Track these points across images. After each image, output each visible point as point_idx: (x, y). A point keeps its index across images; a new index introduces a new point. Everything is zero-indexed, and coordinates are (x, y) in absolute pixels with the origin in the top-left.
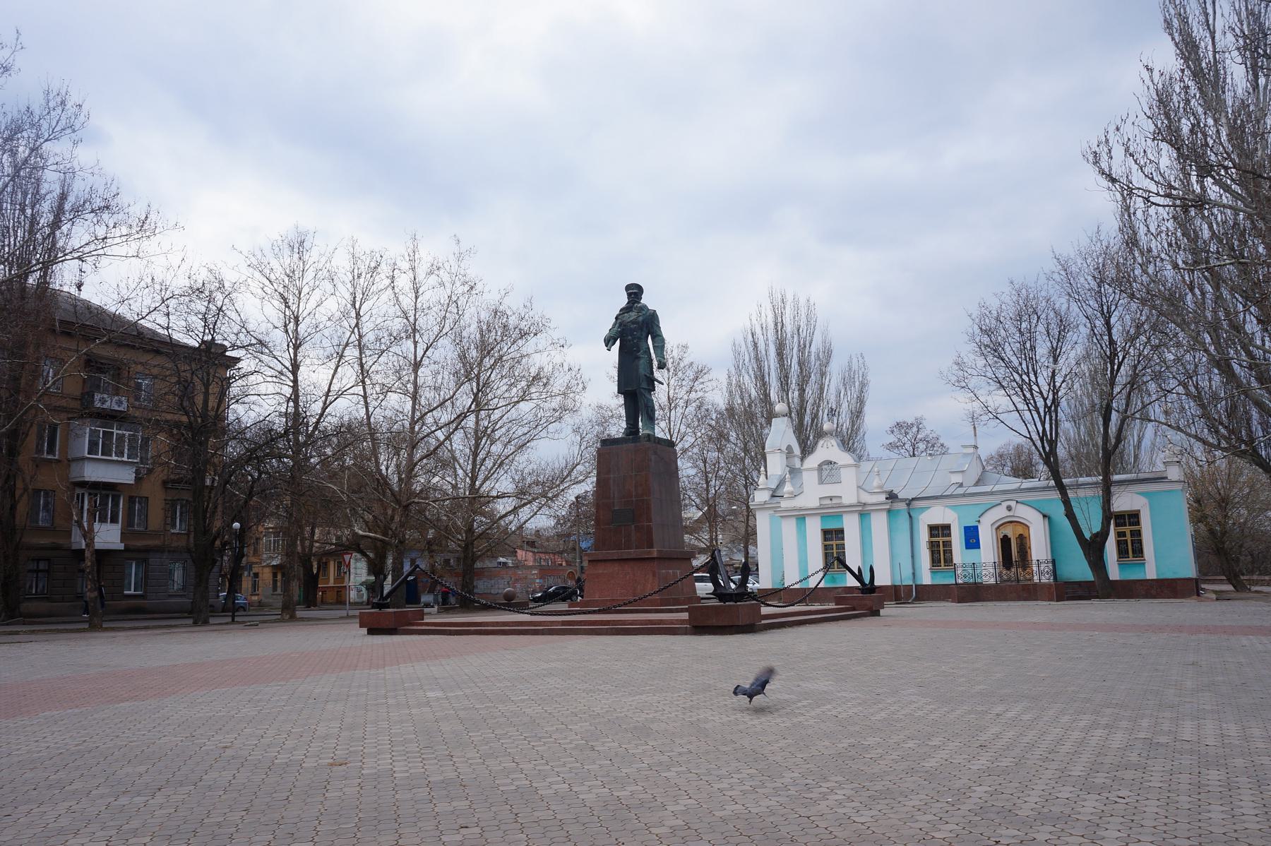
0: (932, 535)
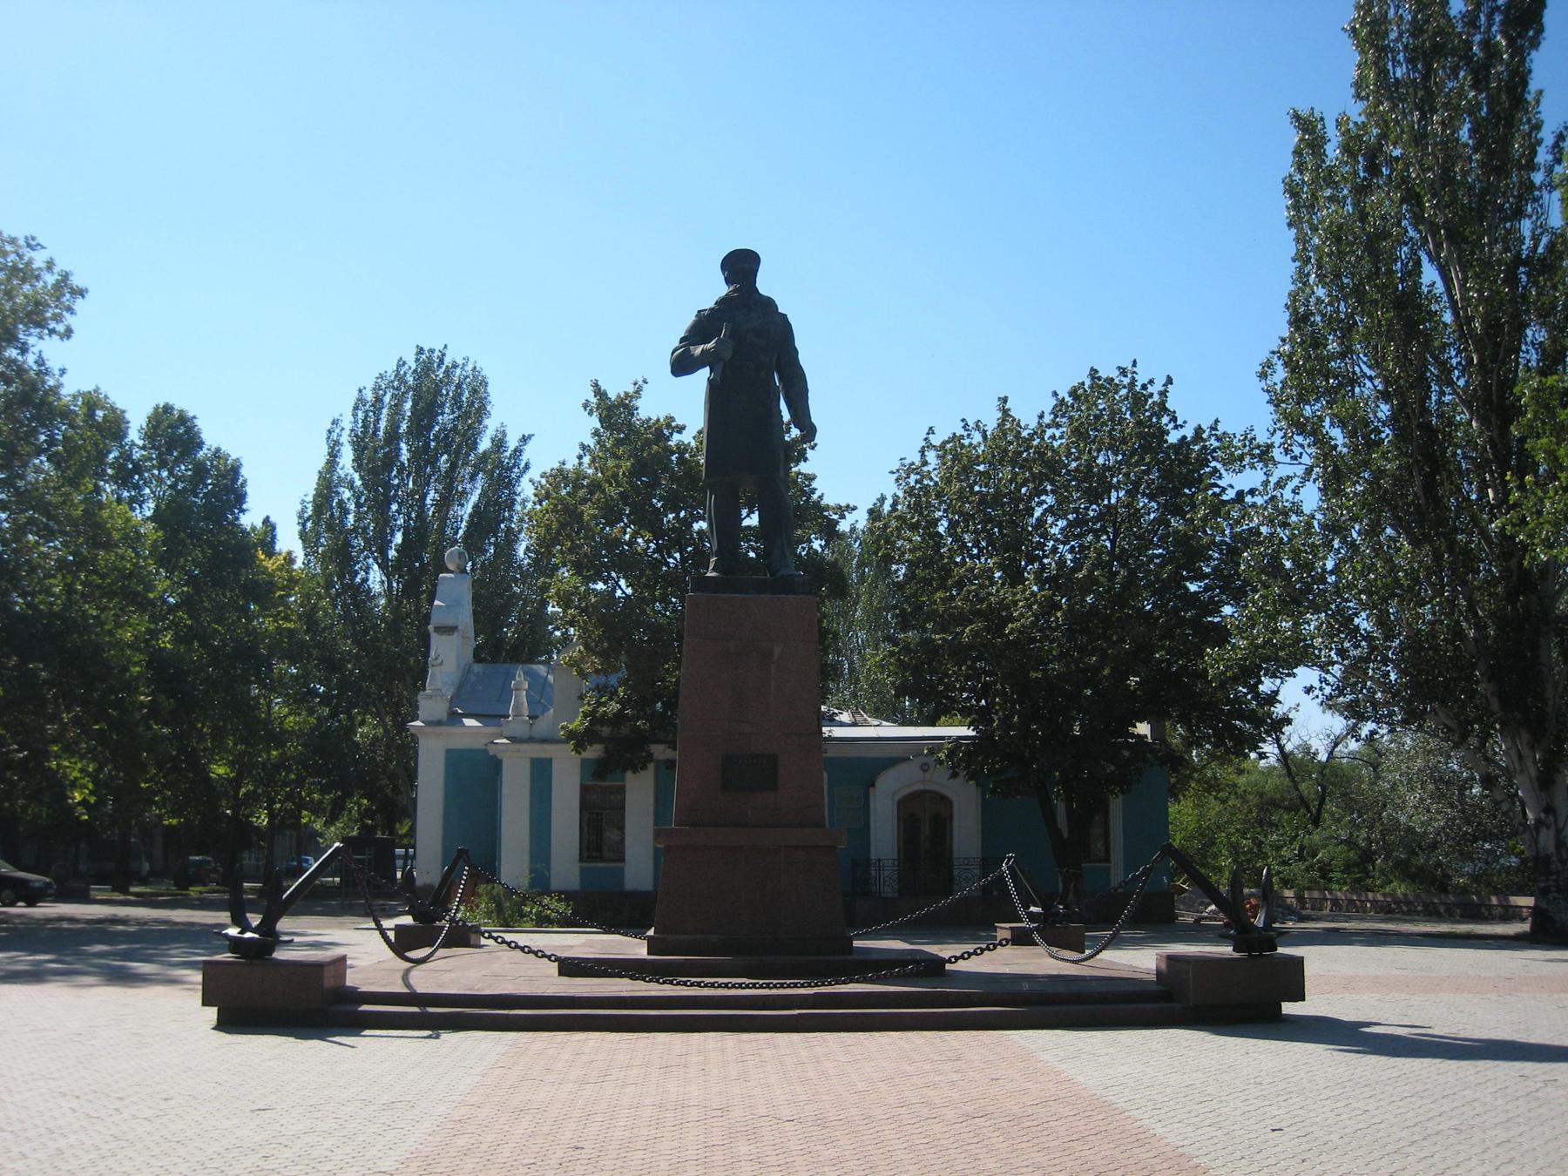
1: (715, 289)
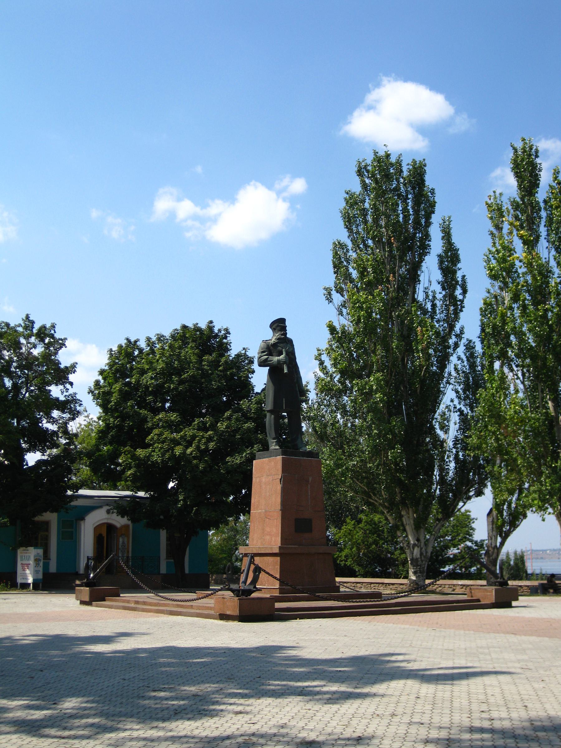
1: (270, 336)
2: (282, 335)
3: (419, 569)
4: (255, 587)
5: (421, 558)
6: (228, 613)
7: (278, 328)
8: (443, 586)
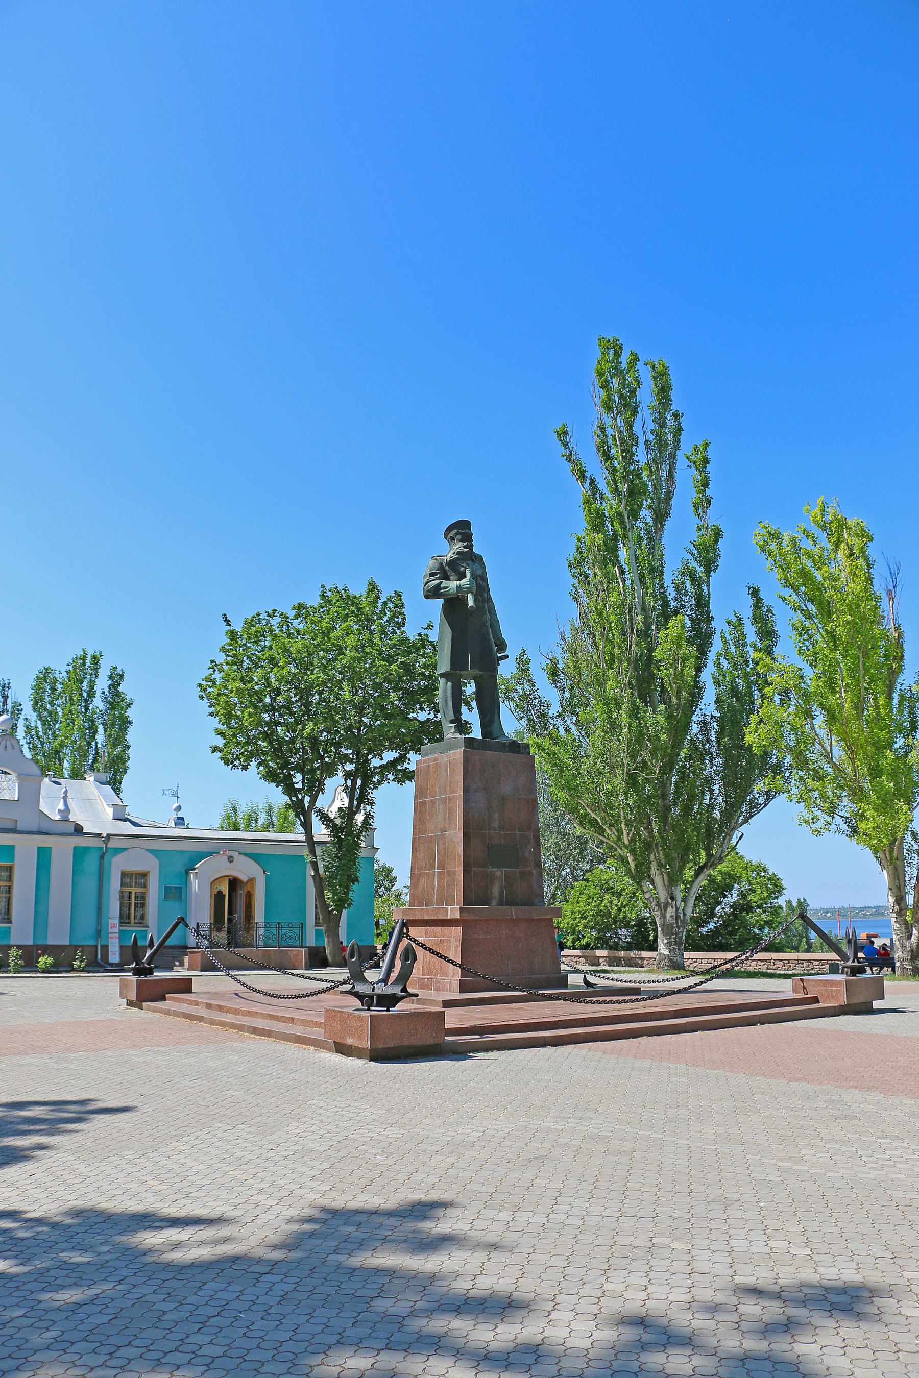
0: (123, 884)
2: (465, 547)
3: (674, 938)
4: (404, 990)
5: (677, 923)
6: (350, 1041)
7: (459, 537)
8: (699, 961)
